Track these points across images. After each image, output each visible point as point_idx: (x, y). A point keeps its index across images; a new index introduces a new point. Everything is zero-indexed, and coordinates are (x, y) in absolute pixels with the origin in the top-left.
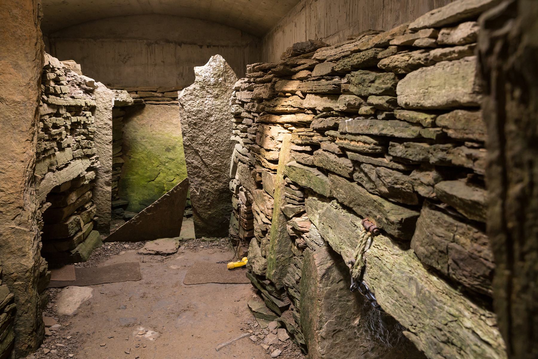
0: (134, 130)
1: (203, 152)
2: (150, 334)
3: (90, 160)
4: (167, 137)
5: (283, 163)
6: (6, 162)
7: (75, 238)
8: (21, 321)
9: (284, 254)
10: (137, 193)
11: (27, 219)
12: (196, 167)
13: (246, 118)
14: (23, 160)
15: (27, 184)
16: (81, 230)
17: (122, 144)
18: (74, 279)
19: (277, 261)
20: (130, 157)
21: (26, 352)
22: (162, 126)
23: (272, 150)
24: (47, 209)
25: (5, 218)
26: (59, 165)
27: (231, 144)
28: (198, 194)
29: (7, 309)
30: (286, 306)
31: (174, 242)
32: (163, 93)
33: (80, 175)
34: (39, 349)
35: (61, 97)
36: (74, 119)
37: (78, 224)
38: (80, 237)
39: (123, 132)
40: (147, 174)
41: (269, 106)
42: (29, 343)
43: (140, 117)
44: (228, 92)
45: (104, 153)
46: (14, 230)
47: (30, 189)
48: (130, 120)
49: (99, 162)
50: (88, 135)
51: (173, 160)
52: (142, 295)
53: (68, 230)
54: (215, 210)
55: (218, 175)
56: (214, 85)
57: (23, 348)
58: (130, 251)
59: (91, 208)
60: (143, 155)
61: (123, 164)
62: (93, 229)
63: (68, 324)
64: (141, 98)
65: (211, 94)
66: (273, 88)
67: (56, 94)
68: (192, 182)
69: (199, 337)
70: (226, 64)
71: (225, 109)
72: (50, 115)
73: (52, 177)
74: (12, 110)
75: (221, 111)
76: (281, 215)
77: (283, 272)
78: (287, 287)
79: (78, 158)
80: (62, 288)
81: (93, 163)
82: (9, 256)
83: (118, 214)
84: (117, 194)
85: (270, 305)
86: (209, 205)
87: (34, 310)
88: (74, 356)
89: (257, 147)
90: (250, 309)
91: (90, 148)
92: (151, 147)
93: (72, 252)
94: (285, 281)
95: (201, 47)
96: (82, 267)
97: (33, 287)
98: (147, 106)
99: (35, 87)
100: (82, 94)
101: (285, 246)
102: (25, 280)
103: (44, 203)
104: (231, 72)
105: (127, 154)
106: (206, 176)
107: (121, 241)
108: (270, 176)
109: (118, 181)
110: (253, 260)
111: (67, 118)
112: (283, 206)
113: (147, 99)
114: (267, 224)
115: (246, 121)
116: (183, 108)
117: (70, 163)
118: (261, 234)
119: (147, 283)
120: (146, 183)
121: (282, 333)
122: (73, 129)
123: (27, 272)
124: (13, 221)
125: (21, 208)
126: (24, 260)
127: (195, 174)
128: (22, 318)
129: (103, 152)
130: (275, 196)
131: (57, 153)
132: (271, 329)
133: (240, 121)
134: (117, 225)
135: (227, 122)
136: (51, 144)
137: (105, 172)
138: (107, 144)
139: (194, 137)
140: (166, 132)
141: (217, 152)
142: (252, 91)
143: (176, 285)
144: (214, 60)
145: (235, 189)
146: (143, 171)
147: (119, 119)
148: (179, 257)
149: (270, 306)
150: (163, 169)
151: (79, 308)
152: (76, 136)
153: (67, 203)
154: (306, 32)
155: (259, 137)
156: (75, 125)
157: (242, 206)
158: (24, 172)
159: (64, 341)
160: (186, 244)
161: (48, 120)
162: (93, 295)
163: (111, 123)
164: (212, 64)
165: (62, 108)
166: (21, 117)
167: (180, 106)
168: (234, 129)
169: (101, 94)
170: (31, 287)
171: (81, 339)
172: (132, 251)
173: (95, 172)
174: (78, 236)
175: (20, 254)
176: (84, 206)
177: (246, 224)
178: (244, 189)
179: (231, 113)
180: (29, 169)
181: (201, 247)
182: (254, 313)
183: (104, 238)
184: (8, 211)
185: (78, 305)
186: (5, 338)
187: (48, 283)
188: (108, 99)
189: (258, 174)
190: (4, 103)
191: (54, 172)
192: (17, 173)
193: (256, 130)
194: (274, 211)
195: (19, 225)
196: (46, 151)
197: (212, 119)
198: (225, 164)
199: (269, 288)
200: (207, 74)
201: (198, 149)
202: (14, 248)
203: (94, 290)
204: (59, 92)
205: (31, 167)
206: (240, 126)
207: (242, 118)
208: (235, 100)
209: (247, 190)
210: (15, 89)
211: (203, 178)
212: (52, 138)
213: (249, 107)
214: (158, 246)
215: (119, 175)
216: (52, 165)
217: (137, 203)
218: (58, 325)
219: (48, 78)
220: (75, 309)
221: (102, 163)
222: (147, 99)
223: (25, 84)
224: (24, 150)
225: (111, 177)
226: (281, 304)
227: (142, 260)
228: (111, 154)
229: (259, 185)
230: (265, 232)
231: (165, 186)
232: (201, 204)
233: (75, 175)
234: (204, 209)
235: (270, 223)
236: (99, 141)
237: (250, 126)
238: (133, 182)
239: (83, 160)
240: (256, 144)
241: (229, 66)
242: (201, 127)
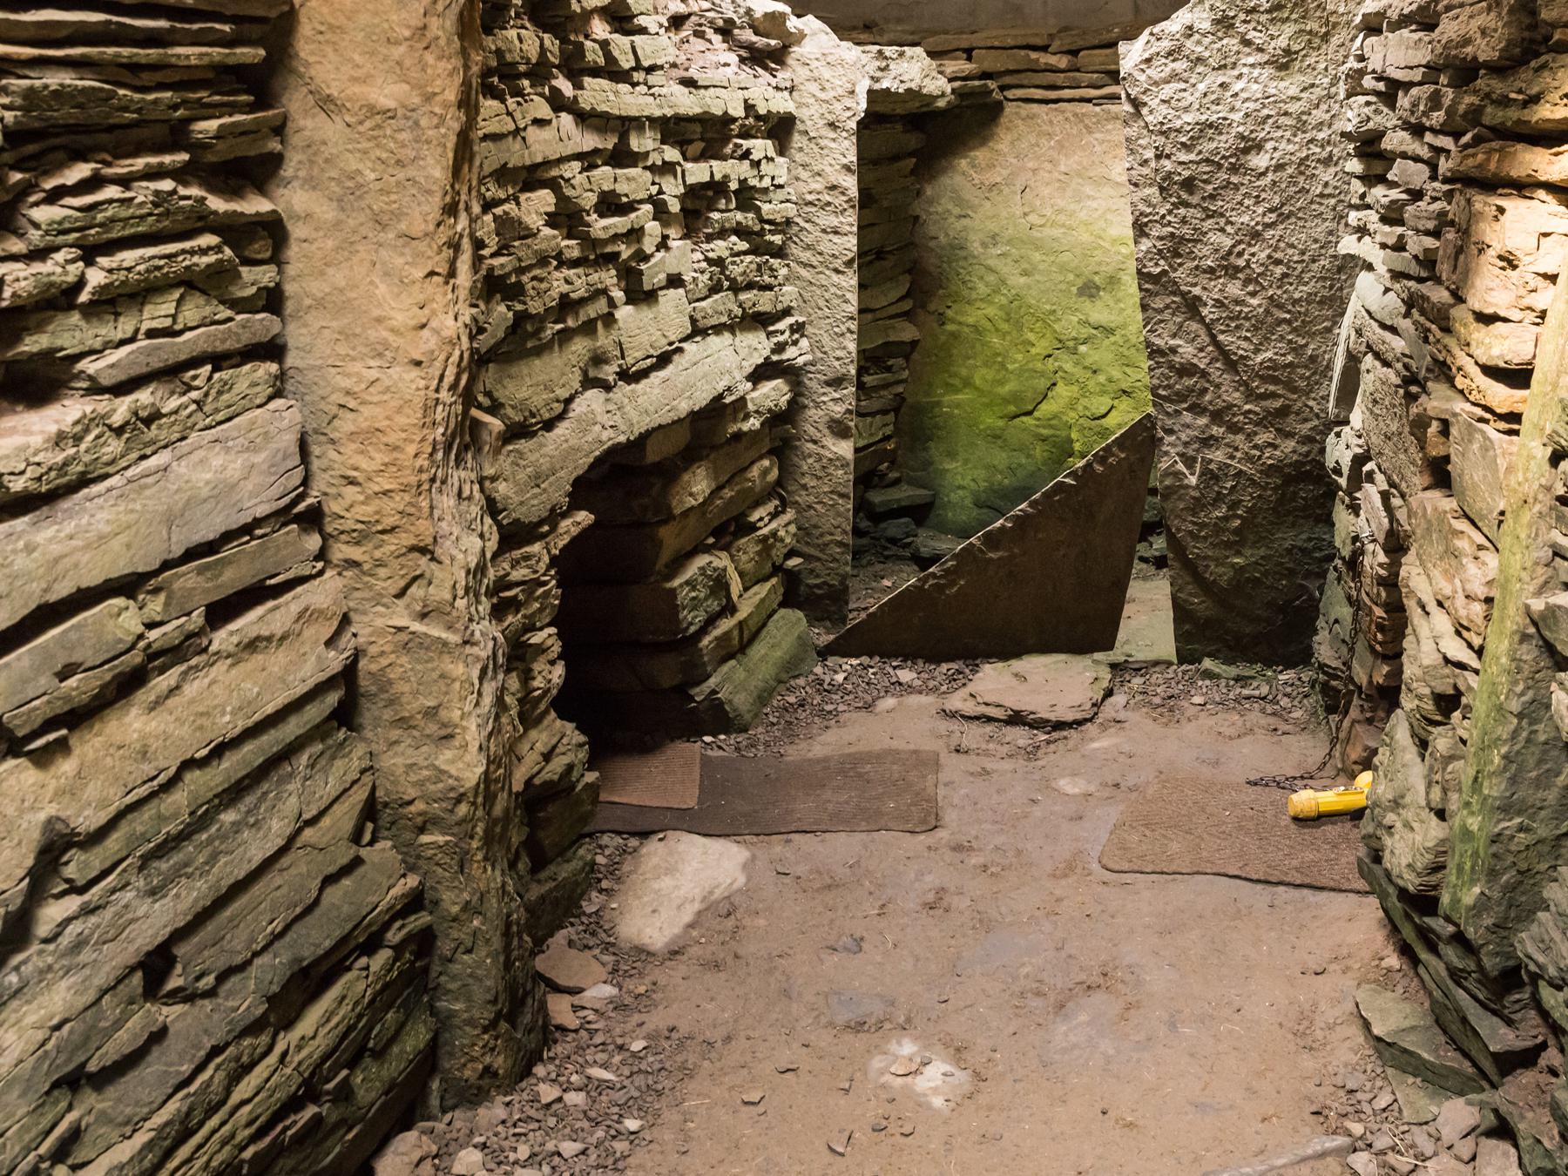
0: (957, 211)
1: (1219, 304)
2: (936, 1080)
4: (1085, 237)
5: (1555, 386)
6: (357, 367)
7: (706, 641)
8: (454, 978)
9: (1532, 818)
10: (966, 462)
11: (448, 597)
12: (1187, 370)
13: (1404, 156)
14: (418, 357)
15: (440, 455)
16: (729, 609)
17: (903, 262)
18: (691, 802)
19: (1494, 848)
20: (942, 320)
21: (479, 1088)
22: (1069, 193)
23: (1505, 320)
24: (574, 540)
25: (371, 588)
26: (630, 360)
27: (1340, 270)
28: (1193, 480)
29: (394, 936)
30: (1526, 1051)
31: (1090, 675)
32: (1074, 53)
33: (721, 396)
34: (523, 1084)
35: (634, 85)
36: (698, 173)
37: (719, 584)
38: (727, 634)
39: (917, 218)
40: (1007, 388)
41: (1505, 102)
43: (980, 155)
44: (1335, 41)
46: (404, 637)
47: (456, 476)
48: (944, 171)
49: (804, 343)
50: (761, 233)
51: (1109, 331)
52: (931, 897)
53: (675, 609)
54: (1262, 552)
55: (1278, 404)
57: (467, 1073)
58: (914, 700)
59: (774, 525)
60: (991, 311)
61: (914, 344)
62: (782, 605)
63: (642, 989)
64: (986, 75)
67: (613, 72)
68: (1170, 432)
69: (1130, 1125)
71: (1319, 115)
72: (589, 160)
74: (365, 145)
75: (1301, 126)
76: (1525, 638)
77: (1519, 900)
78: (1535, 978)
79: (718, 329)
80: (645, 835)
81: (779, 348)
82: (395, 734)
83: (893, 541)
84: (892, 463)
85: (1455, 1028)
86: (1237, 531)
87: (497, 943)
88: (642, 1128)
89: (1439, 295)
90: (1367, 1025)
91: (769, 288)
92: (1023, 280)
93: (692, 692)
94: (1527, 944)
96: (729, 753)
97: (486, 859)
98: (1010, 108)
99: (449, 42)
100: (734, 68)
101: (1538, 784)
102: (455, 830)
103: (564, 515)
105: (932, 307)
106: (1230, 406)
107: (886, 654)
108: (1487, 446)
109: (897, 410)
110: (1390, 818)
111: (668, 168)
112: (1539, 592)
113: (1007, 80)
114: (1461, 666)
115: (1403, 171)
116: (1138, 114)
117: (680, 350)
118: (1429, 706)
119: (958, 848)
120: (1001, 423)
121: (1497, 1160)
123: (458, 801)
124: (401, 603)
125: (423, 550)
126: (448, 754)
127: (1181, 397)
128: (455, 968)
129: (822, 303)
130: (1505, 542)
131: (624, 313)
132: (1449, 1133)
133: (1378, 168)
134: (887, 583)
135: (1327, 175)
136: (595, 277)
137: (828, 384)
138: (837, 271)
140: (1082, 215)
141: (1280, 307)
142: (1430, 27)
143: (1070, 868)
145: (1346, 471)
146: (990, 374)
147: (901, 164)
148: (1099, 742)
149: (1449, 1024)
150: (1068, 367)
151: (691, 926)
152: (710, 238)
153: (669, 509)
155: (1451, 250)
156: (700, 199)
157: (1370, 547)
158: (426, 408)
159: (617, 1059)
160: (1137, 681)
161: (580, 179)
162: (749, 879)
163: (851, 183)
166: (401, 176)
167: (1128, 108)
168: (1357, 208)
169: (814, 64)
170: (479, 856)
171: (679, 1059)
172: (923, 699)
173: (788, 382)
174: (717, 632)
175: (432, 728)
176: (744, 515)
177: (1381, 628)
178: (1379, 477)
179: (1343, 134)
180: (444, 395)
181: (1198, 700)
182: (1381, 1046)
183: (825, 638)
184: (380, 563)
185: (687, 916)
186: (393, 1040)
187: (585, 819)
188: (839, 84)
189: (1434, 427)
190: (337, 119)
191: (607, 387)
192: (399, 410)
193: (1442, 214)
194: (1496, 613)
195: (423, 616)
197: (1260, 161)
198: (1313, 359)
199: (1451, 953)
201: (1197, 291)
202: (412, 706)
203: (754, 858)
204: (626, 63)
205: (453, 387)
206: (1379, 193)
207: (1388, 158)
208: (1361, 73)
209: (1392, 484)
210: (372, 54)
211: (1217, 417)
213: (1415, 105)
214: (1023, 687)
215: (900, 389)
216: (598, 359)
217: (968, 502)
218: (609, 990)
220: (676, 931)
221: (817, 346)
222: (1009, 78)
223: (407, 33)
224: (422, 316)
226: (1500, 1038)
227: (954, 743)
228: (852, 308)
229: (1440, 474)
230: (1448, 703)
231: (1074, 436)
232: (1203, 526)
233: (701, 398)
234: (1214, 545)
235: (1475, 664)
236: (806, 256)
237: (1417, 195)
238: (951, 416)
239: (739, 337)
240: (1438, 281)
242: (1212, 197)
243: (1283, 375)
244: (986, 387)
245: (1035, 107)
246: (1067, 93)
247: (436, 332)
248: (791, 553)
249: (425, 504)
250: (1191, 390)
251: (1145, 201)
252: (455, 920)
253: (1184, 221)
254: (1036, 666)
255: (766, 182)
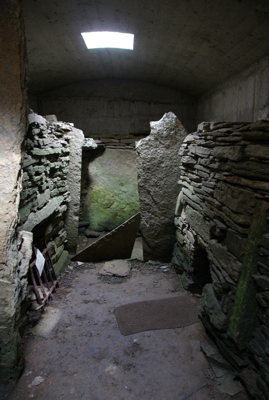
3: (64, 196)
12: (147, 204)
15: (9, 242)
17: (86, 181)
27: (178, 186)
28: (148, 226)
32: (120, 140)
42: (12, 375)
44: (178, 143)
45: (74, 196)
47: (12, 246)
49: (70, 197)
50: (63, 176)
55: (165, 211)
56: (167, 137)
62: (64, 250)
64: (103, 143)
65: (163, 144)
66: (242, 151)
67: (39, 146)
68: (143, 216)
70: (178, 120)
71: (174, 157)
72: (34, 165)
73: (33, 217)
75: (171, 159)
79: (54, 196)
81: (65, 199)
86: (156, 236)
87: (15, 349)
90: (205, 354)
91: (64, 186)
95: (149, 103)
98: (107, 149)
104: (181, 127)
111: (47, 165)
116: (139, 155)
122: (52, 173)
123: (9, 319)
125: (4, 264)
126: (7, 308)
131: (39, 195)
136: (33, 190)
137: (74, 205)
138: (77, 183)
139: (147, 179)
141: (166, 193)
144: (167, 117)
148: (132, 280)
154: (254, 95)
163: (80, 165)
164: (166, 119)
165: (43, 158)
170: (13, 330)
180: (11, 229)
191: (35, 212)
196: (29, 196)
197: (163, 165)
200: (161, 128)
201: (150, 189)
205: (13, 227)
211: (153, 214)
212: (34, 185)
217: (96, 224)
219: (34, 134)
221: (72, 197)
222: (107, 144)
225: (78, 209)
228: (79, 190)
233: (52, 212)
241: (179, 122)
242: (153, 171)
243: (166, 206)
244: (101, 202)
245: (112, 149)
246: (118, 147)
247: (10, 215)
248: (66, 239)
249: (5, 253)
250: (148, 208)
251: (140, 172)
252: (6, 345)
253: (148, 176)
254: (116, 262)
255: (64, 166)
